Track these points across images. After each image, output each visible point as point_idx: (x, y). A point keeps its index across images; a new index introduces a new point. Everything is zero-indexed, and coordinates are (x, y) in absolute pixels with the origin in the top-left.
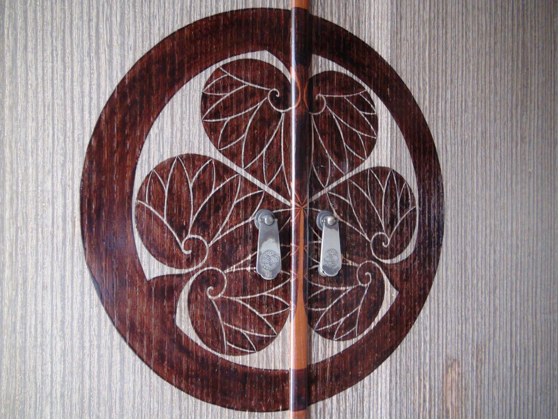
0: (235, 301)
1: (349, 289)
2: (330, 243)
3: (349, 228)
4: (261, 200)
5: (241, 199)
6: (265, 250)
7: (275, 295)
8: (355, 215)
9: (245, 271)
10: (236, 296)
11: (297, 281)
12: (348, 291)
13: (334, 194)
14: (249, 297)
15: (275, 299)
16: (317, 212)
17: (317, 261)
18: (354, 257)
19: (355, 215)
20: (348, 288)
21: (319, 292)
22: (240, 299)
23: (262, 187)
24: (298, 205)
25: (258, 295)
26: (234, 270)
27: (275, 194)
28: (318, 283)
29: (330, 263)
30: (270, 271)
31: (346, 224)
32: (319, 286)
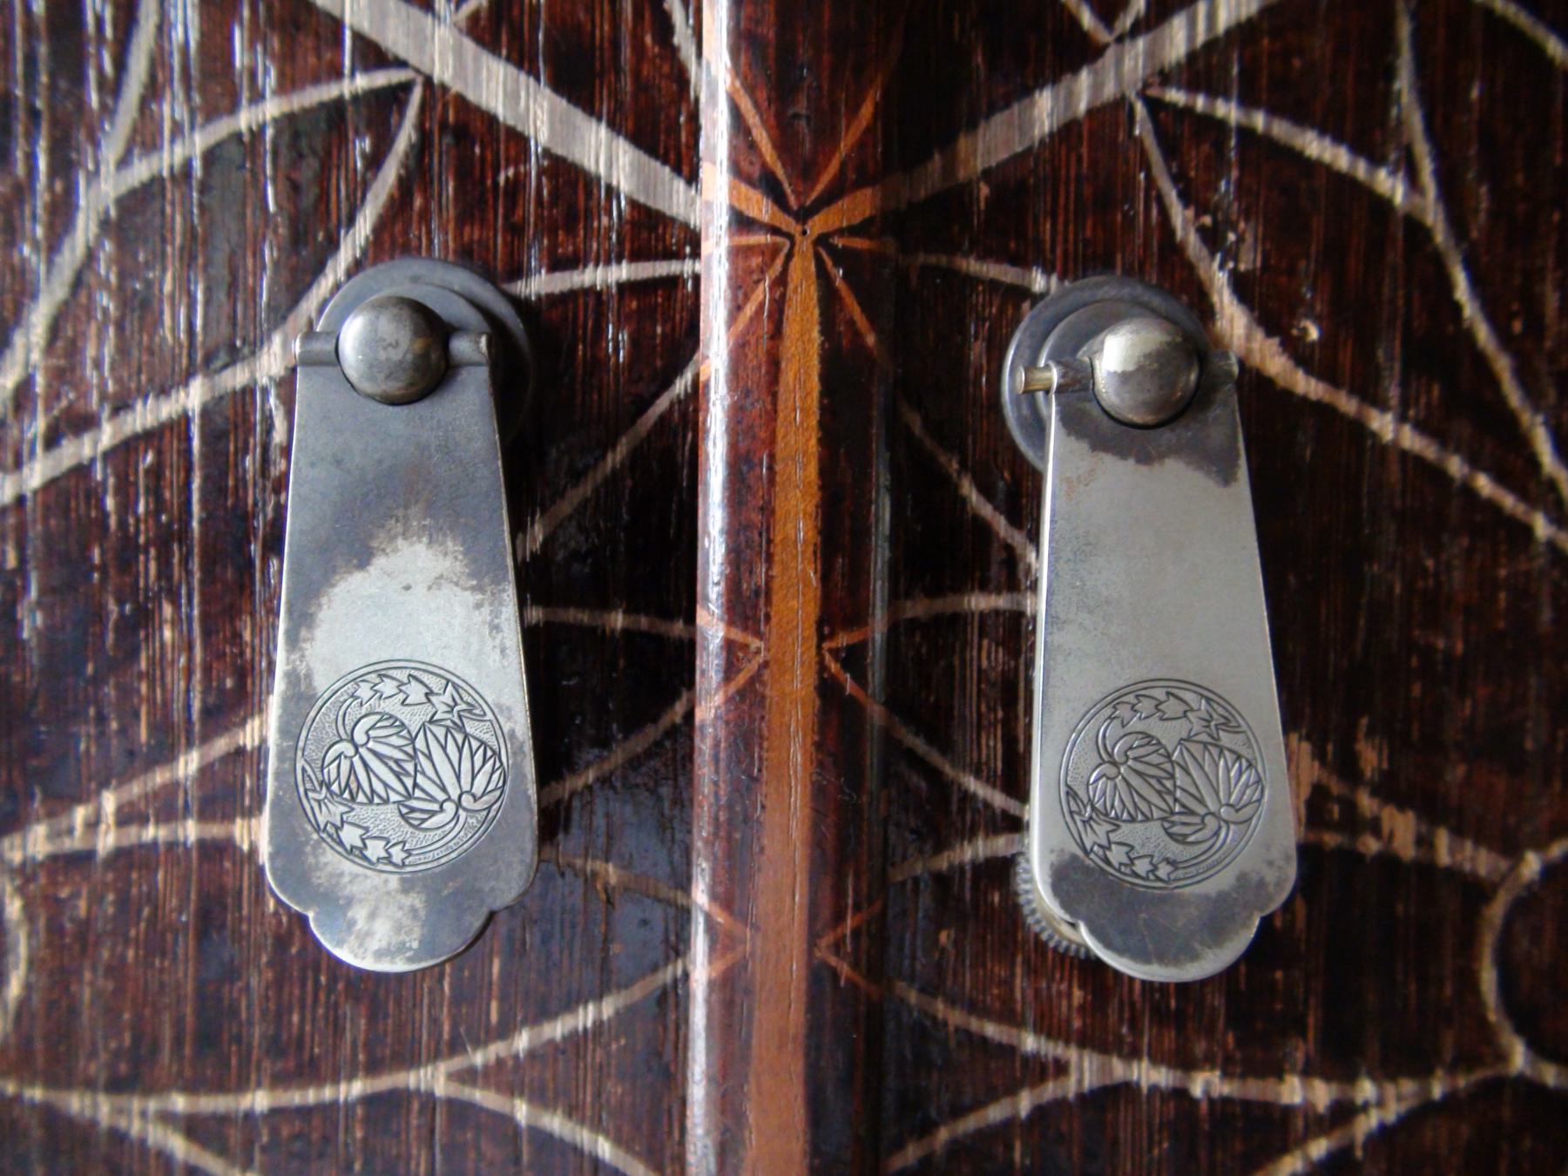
0: (118, 1137)
1: (1380, 1102)
2: (1141, 621)
3: (1394, 474)
4: (390, 172)
5: (170, 157)
6: (354, 662)
7: (541, 1098)
8: (1483, 334)
9: (216, 851)
10: (116, 1086)
11: (731, 991)
12: (1367, 1123)
13: (1228, 111)
14: (260, 1100)
15: (543, 1139)
16: (1021, 294)
17: (999, 799)
18: (1457, 772)
19: (1483, 334)
20: (1366, 1089)
21: (1025, 1103)
22: (167, 1118)
23: (395, 39)
24: (761, 208)
25: (356, 1088)
26: (107, 841)
27: (534, 110)
28: (1008, 1016)
29: (1147, 837)
30: (407, 886)
31: (1358, 429)
32: (1030, 1042)
